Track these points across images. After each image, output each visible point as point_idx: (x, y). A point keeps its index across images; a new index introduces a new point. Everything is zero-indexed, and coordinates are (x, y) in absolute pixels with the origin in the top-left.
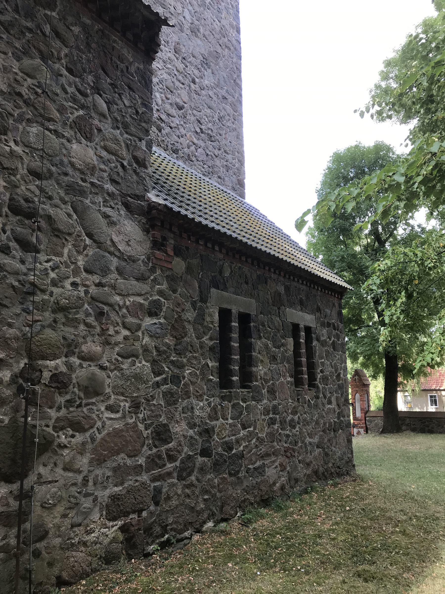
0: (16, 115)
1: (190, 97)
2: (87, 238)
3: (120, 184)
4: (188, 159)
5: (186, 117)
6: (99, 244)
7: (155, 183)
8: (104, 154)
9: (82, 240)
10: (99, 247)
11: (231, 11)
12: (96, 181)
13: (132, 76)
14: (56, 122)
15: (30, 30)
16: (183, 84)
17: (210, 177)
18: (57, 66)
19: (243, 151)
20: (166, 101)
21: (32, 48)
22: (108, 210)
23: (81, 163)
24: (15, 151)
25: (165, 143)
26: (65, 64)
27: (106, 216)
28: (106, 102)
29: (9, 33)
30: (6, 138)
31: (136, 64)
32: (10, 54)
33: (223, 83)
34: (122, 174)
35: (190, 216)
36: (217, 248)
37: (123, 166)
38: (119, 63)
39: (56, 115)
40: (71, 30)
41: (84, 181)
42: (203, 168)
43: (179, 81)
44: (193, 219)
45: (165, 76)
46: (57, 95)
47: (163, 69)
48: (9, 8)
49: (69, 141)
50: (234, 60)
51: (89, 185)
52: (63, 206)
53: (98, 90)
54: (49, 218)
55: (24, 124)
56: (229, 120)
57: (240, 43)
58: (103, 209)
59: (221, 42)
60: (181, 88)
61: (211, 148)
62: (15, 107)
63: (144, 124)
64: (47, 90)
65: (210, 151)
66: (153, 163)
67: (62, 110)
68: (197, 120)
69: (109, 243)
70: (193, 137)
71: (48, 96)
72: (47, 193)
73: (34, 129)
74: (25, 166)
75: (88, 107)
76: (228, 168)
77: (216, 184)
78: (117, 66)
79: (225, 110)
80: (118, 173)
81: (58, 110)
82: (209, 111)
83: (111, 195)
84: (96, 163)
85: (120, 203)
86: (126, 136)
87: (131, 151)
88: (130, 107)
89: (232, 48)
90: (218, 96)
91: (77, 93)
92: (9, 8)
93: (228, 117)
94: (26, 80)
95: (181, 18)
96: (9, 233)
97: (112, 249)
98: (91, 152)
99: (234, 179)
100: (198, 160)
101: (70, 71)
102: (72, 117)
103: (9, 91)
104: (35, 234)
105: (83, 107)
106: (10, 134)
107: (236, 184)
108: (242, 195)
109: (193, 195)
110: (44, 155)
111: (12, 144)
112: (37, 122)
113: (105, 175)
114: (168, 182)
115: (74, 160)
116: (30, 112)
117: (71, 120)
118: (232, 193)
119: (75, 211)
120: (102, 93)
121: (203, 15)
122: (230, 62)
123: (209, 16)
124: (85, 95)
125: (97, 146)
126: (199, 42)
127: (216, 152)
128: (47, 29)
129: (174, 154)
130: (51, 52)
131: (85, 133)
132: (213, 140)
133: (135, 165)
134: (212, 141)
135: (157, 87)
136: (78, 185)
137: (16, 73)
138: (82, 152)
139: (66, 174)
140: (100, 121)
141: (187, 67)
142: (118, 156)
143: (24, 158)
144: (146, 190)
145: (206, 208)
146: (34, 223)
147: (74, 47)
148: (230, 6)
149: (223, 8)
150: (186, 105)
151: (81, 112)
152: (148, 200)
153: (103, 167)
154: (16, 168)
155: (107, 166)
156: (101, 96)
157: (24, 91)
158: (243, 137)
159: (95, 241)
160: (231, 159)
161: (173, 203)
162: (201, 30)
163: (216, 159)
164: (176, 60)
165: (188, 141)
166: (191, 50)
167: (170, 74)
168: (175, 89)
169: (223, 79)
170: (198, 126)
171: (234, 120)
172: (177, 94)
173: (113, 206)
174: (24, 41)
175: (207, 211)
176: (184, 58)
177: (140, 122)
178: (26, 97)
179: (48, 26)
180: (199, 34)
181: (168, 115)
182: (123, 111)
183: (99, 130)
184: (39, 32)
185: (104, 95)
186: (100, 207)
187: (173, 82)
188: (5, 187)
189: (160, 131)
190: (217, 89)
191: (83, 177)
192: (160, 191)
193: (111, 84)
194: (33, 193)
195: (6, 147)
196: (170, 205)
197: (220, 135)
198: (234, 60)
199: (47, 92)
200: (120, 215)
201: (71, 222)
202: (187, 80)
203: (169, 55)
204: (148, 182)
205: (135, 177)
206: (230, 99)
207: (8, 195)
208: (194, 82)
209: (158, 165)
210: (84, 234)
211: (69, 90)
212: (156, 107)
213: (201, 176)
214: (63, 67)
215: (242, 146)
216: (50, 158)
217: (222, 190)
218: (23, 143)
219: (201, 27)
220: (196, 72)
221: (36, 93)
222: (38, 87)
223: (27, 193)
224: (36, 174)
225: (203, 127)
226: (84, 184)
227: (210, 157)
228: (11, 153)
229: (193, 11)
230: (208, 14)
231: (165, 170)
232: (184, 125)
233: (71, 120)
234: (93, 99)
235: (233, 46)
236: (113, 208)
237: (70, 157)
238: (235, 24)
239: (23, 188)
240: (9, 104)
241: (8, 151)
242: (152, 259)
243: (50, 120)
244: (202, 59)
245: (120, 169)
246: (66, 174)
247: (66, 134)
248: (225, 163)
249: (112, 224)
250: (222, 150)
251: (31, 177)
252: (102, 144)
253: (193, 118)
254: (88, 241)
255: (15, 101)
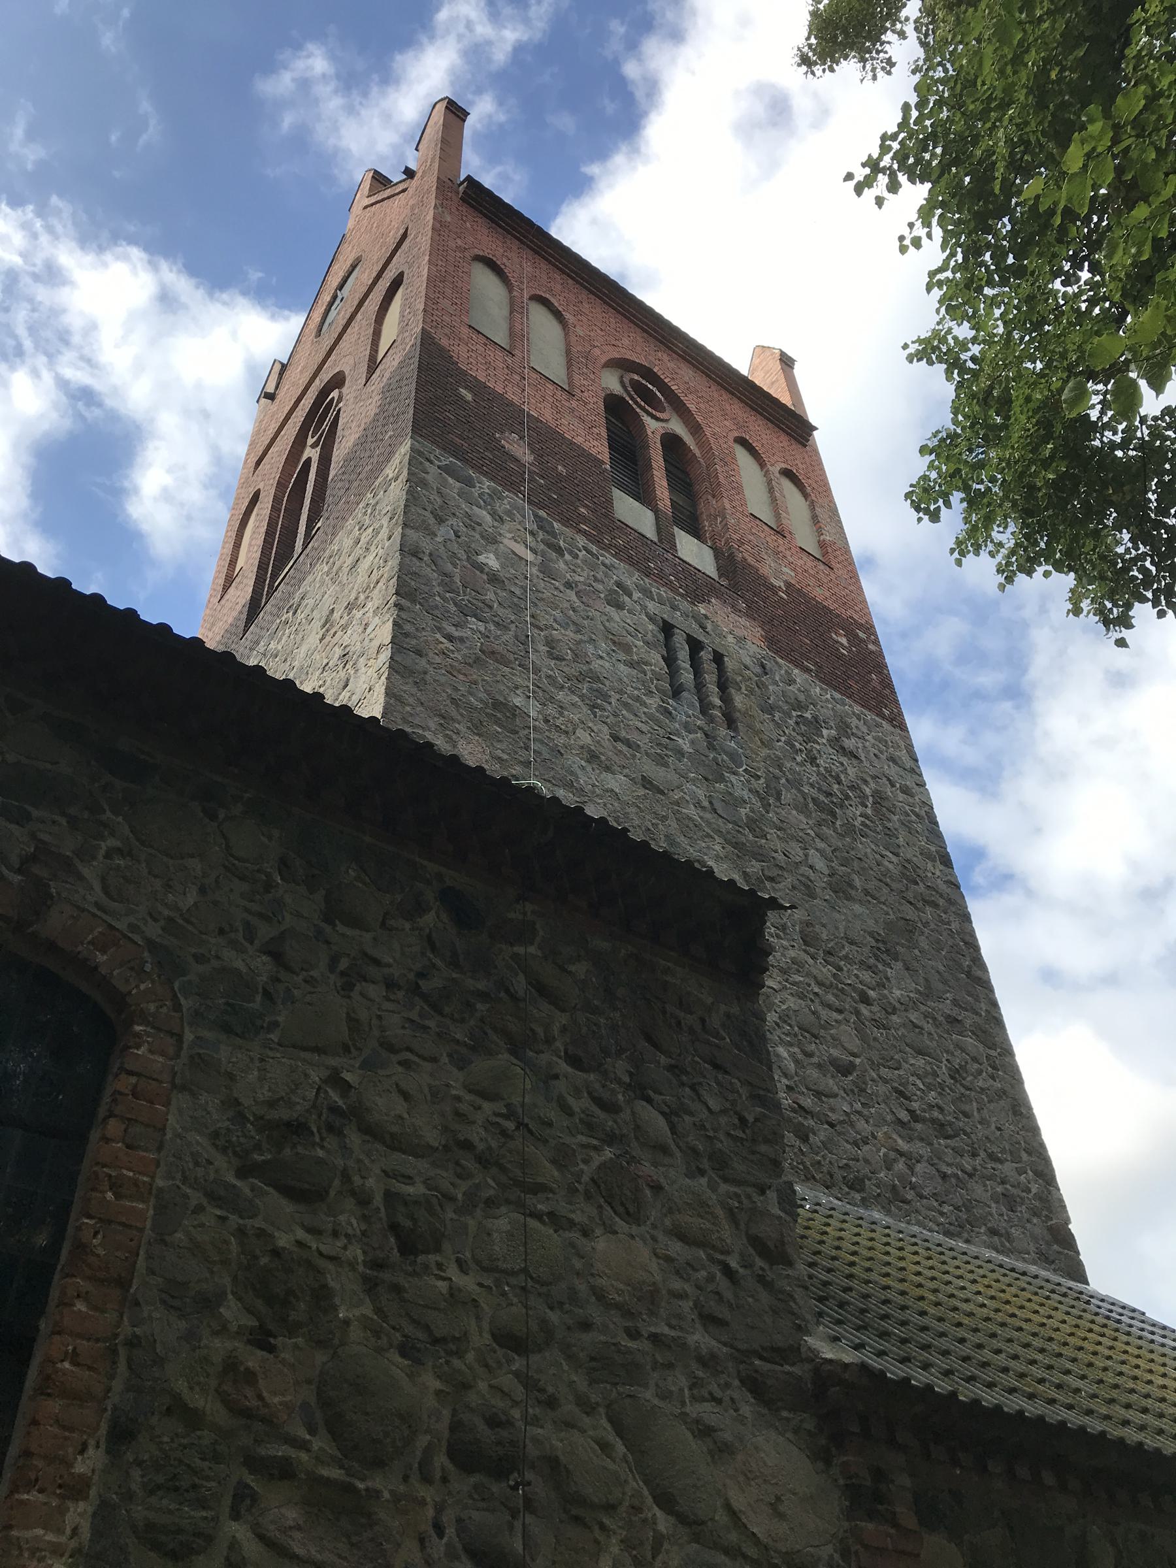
0: (460, 1196)
1: (863, 1038)
2: (659, 1513)
3: (727, 1324)
4: (894, 1199)
5: (864, 1090)
6: (692, 1524)
7: (821, 1300)
8: (676, 1248)
9: (645, 1521)
10: (696, 1538)
11: (919, 827)
12: (666, 1330)
13: (717, 1035)
14: (552, 1191)
15: (484, 996)
16: (840, 1011)
17: (965, 1235)
18: (545, 1058)
19: (1042, 1145)
20: (806, 1061)
21: (489, 1032)
22: (706, 1411)
23: (621, 1286)
24: (460, 1290)
25: (825, 1169)
26: (562, 1049)
27: (704, 1431)
28: (663, 1113)
29: (441, 1014)
30: (439, 1258)
31: (723, 1008)
32: (445, 1059)
33: (941, 986)
34: (728, 1295)
35: (942, 1387)
36: (1049, 1479)
37: (728, 1272)
38: (682, 1014)
39: (549, 1173)
40: (570, 973)
41: (634, 1334)
42: (942, 1214)
43: (830, 1007)
44: (954, 1394)
45: (792, 1003)
46: (550, 1124)
47: (785, 988)
48: (438, 962)
49: (586, 1233)
50: (953, 926)
51: (646, 1345)
52: (587, 1421)
53: (641, 1090)
54: (553, 1466)
55: (479, 1212)
56: (980, 1072)
57: (958, 887)
58: (693, 1410)
59: (910, 895)
60: (836, 1021)
61: (949, 1156)
62: (459, 1176)
63: (763, 1148)
64: (526, 1120)
65: (948, 1165)
66: (803, 1237)
67: (562, 1158)
68: (896, 1090)
69: (721, 1517)
70: (895, 1136)
71: (531, 1132)
72: (542, 1390)
73: (503, 1222)
74: (486, 1325)
75: (623, 1136)
76: (1011, 1203)
77: (988, 1254)
78: (679, 1023)
79: (963, 1050)
80: (718, 1293)
81: (554, 1162)
82: (920, 1062)
83: (708, 1361)
84: (658, 1278)
85: (736, 1383)
86: (724, 1187)
87: (742, 1226)
88: (724, 1112)
89: (941, 902)
90: (935, 1019)
91: (597, 1111)
92: (438, 962)
93: (976, 1066)
94: (480, 1108)
95: (804, 869)
96: (450, 1531)
97: (733, 1537)
98: (643, 1253)
99: (1037, 1227)
100: (921, 1197)
101: (575, 1062)
102: (588, 1171)
103: (443, 1142)
104: (518, 1524)
105: (611, 1139)
106: (447, 1246)
107: (1048, 1244)
108: (1077, 1272)
109: (932, 1310)
110: (530, 1283)
111: (453, 1272)
112: (508, 1202)
113: (686, 1306)
114: (854, 1284)
115: (602, 1282)
116: (490, 1181)
117: (585, 1178)
118: (1043, 1273)
119: (620, 1433)
120: (651, 1093)
121: (853, 853)
122: (945, 934)
123: (869, 850)
124: (610, 1108)
125: (655, 1233)
126: (857, 908)
127: (967, 1163)
128: (520, 984)
129: (852, 1192)
130: (532, 1030)
131: (622, 1204)
132: (951, 1132)
133: (759, 1262)
134: (947, 1137)
135: (778, 1032)
136: (619, 1351)
137: (458, 1099)
138: (623, 1255)
139: (586, 1326)
140: (655, 1164)
141: (840, 969)
142: (713, 1247)
143: (481, 1301)
144: (799, 1328)
145: (980, 1346)
146: (514, 1488)
147: (578, 1007)
148: (913, 818)
149: (897, 825)
150: (858, 1061)
151: (608, 1153)
152: (813, 1358)
153: (677, 1285)
154: (465, 1334)
155: (687, 1280)
156: (649, 1101)
157: (477, 1134)
158: (1030, 1108)
159: (682, 1519)
160: (1014, 1173)
161: (881, 1354)
162: (857, 882)
163: (971, 1184)
164: (811, 961)
165: (883, 1150)
166: (842, 929)
167: (802, 997)
168: (822, 1027)
169: (937, 977)
170: (901, 1105)
171: (994, 1068)
172: (829, 1038)
173: (718, 1393)
174: (472, 1023)
175: (987, 1355)
176: (829, 953)
177: (757, 1144)
178: (481, 1146)
179: (521, 977)
180: (853, 893)
181: (818, 1094)
182: (708, 1126)
183: (657, 1188)
184: (502, 994)
185: (657, 1098)
186: (683, 1404)
187: (813, 1013)
188: (438, 1393)
189: (805, 1139)
190: (929, 1003)
191: (630, 1324)
192: (839, 1322)
193: (671, 1068)
194: (505, 1394)
195: (440, 1283)
196: (875, 1363)
197: (966, 1115)
198: (954, 926)
199: (527, 1125)
200: (742, 1420)
201: (612, 1466)
202: (849, 999)
203: (792, 953)
204: (801, 1303)
205: (765, 1297)
206: (969, 1020)
207: (446, 1413)
208: (865, 1000)
209: (818, 1237)
210: (649, 1500)
211: (575, 1104)
212: (785, 1081)
213: (940, 1238)
214: (560, 1057)
215: (1035, 1130)
216: (544, 1289)
217: (1013, 1270)
218: (478, 1262)
219: (855, 877)
220: (866, 976)
221: (504, 1133)
222: (507, 1117)
223: (493, 1402)
224: (513, 1342)
225: (915, 1105)
226: (632, 1344)
227: (953, 1181)
228: (452, 1295)
229: (829, 850)
230: (865, 847)
231: (838, 1248)
232: (865, 1112)
233: (585, 1178)
234: (633, 1113)
235: (941, 896)
236: (719, 1401)
237: (592, 1275)
238: (933, 849)
239: (482, 1386)
240: (445, 1174)
241: (444, 1291)
242: (856, 1552)
243: (538, 1189)
244: (874, 944)
245: (722, 1282)
246: (586, 1326)
247: (577, 1217)
248: (999, 1189)
249: (722, 1451)
250: (983, 1154)
251: (500, 1352)
252: (668, 1222)
253: (882, 1089)
254: (664, 1522)
255: (457, 1163)
